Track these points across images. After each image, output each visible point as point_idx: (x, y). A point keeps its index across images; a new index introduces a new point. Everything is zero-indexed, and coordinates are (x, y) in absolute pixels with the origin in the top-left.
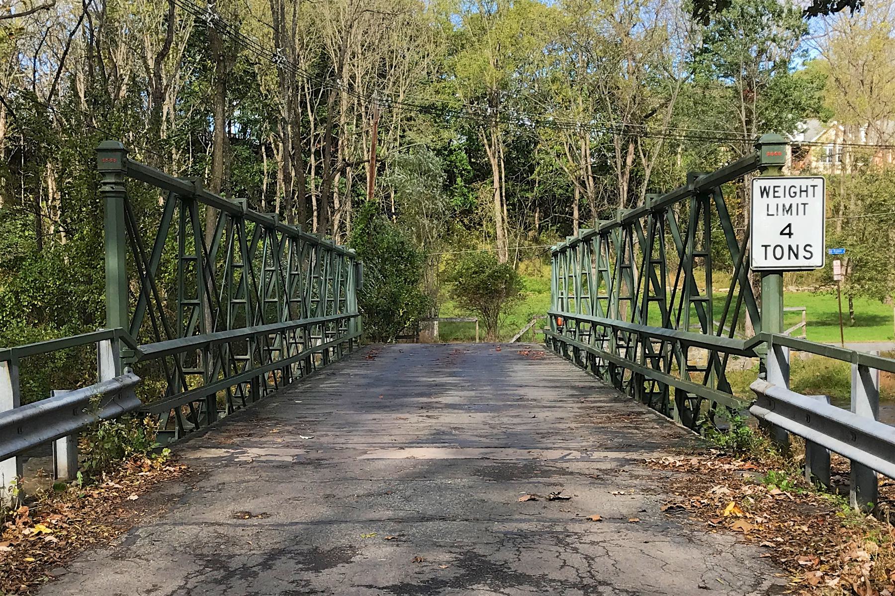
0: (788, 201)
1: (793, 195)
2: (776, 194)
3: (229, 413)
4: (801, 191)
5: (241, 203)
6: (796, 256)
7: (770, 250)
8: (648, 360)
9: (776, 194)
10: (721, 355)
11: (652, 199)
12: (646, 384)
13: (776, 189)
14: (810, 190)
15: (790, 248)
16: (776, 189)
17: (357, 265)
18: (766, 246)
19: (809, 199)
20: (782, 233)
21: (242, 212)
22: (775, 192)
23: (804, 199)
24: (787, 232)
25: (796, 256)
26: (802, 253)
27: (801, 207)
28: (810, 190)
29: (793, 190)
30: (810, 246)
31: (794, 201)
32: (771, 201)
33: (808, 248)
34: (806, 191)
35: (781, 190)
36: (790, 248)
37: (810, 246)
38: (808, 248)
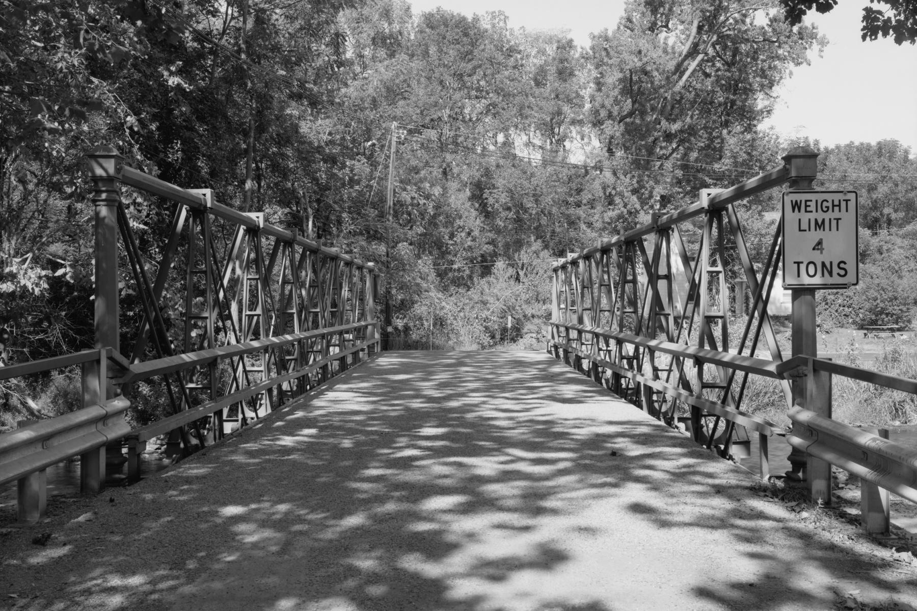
0: (820, 216)
1: (825, 209)
2: (808, 209)
3: (242, 425)
4: (834, 206)
5: (204, 195)
6: (831, 274)
7: (803, 267)
8: (625, 361)
9: (808, 209)
10: (681, 358)
11: (709, 195)
12: (623, 381)
13: (808, 203)
14: (843, 204)
15: (823, 264)
16: (808, 203)
17: (375, 279)
18: (798, 263)
19: (843, 214)
20: (814, 249)
21: (205, 206)
22: (806, 206)
23: (836, 214)
24: (819, 245)
25: (831, 274)
26: (836, 270)
27: (834, 223)
28: (843, 204)
29: (825, 204)
30: (845, 263)
31: (827, 216)
32: (805, 217)
33: (842, 265)
34: (839, 206)
35: (813, 204)
36: (823, 264)
37: (845, 263)
38: (842, 265)
